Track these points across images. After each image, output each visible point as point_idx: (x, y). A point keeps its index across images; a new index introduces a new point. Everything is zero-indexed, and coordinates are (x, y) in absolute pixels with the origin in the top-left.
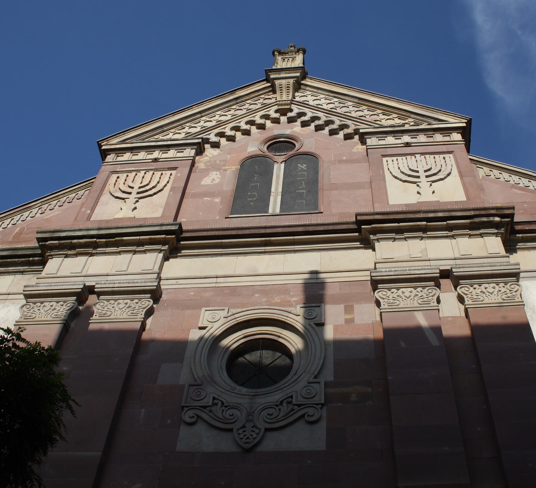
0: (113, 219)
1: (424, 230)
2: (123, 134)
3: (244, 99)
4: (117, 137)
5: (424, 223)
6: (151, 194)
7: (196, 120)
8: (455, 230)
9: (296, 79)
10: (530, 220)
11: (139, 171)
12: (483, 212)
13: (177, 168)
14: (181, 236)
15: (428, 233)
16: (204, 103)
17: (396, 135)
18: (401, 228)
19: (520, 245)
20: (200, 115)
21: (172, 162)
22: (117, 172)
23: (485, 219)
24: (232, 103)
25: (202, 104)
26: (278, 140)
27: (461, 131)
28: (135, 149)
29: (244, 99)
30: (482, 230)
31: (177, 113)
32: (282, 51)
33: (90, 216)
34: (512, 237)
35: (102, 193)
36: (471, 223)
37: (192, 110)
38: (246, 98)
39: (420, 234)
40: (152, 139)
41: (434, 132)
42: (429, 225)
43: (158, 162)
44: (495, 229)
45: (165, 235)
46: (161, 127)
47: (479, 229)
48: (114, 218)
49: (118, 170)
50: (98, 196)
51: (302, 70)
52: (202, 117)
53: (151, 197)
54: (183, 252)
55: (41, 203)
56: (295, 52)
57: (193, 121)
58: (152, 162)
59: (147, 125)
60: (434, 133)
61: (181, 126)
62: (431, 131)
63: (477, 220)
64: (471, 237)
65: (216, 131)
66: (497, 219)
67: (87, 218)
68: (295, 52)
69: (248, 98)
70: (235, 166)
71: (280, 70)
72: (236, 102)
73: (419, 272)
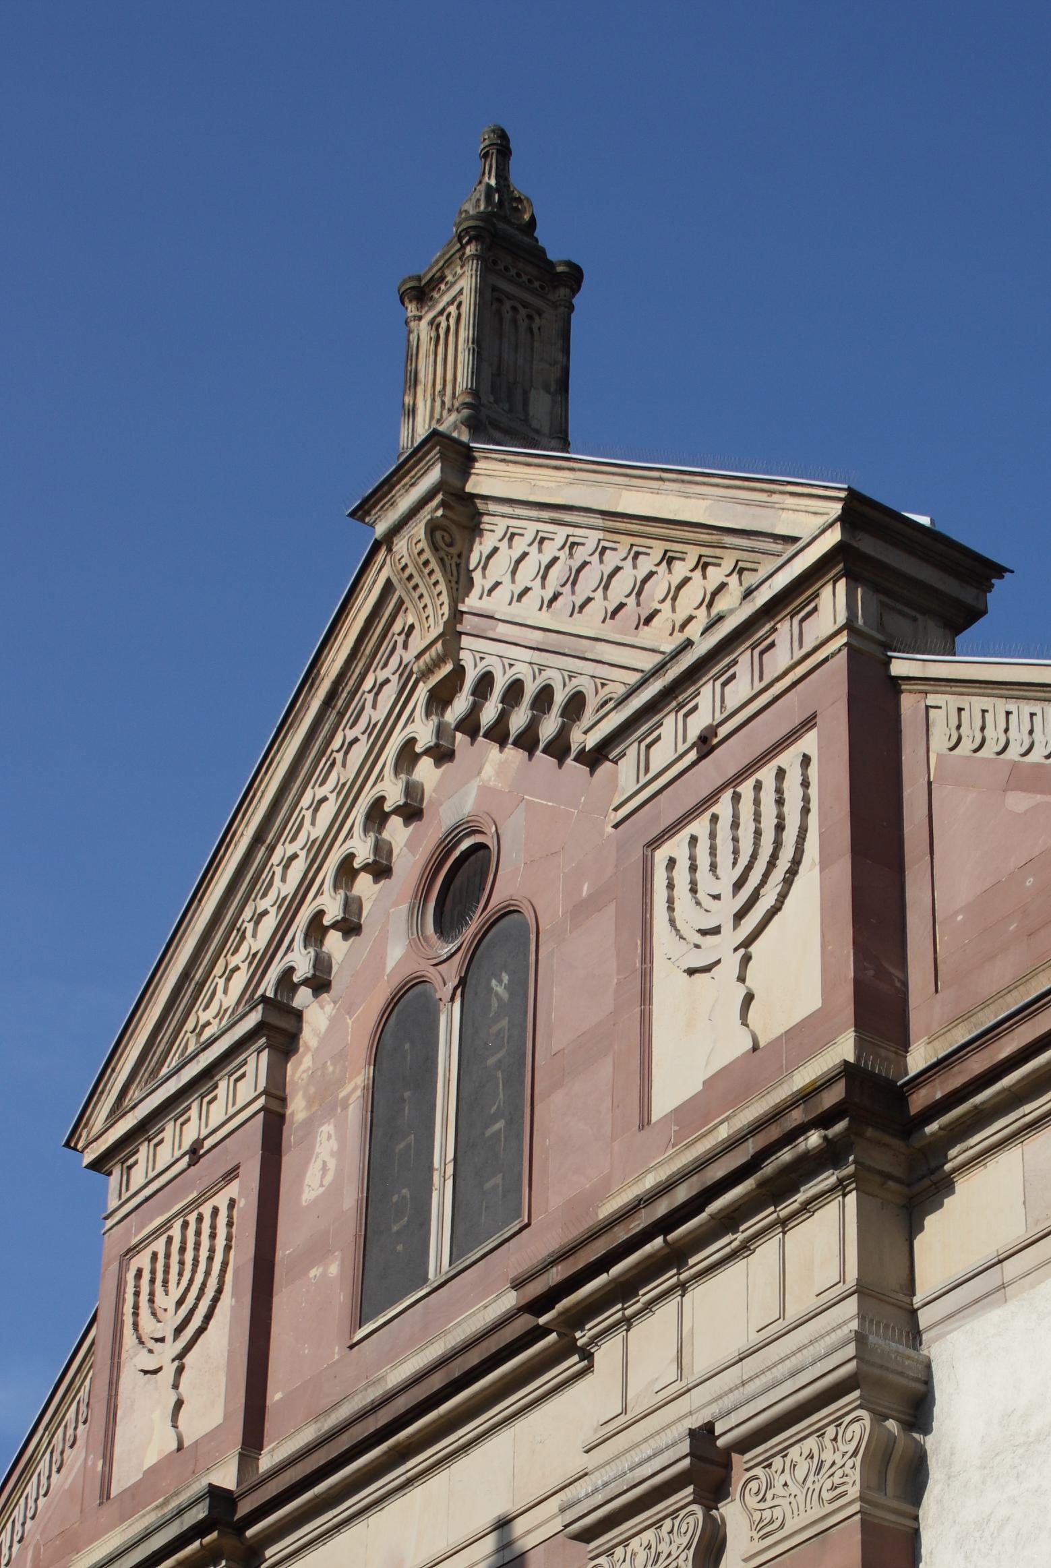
0: (141, 1476)
1: (676, 1257)
2: (109, 1070)
3: (351, 682)
4: (102, 1093)
5: (658, 1242)
6: (200, 1327)
7: (264, 876)
8: (743, 1224)
9: (440, 497)
10: (940, 1057)
11: (167, 1225)
12: (774, 1133)
13: (237, 1167)
14: (235, 1519)
15: (692, 1261)
16: (255, 786)
17: (680, 699)
18: (622, 1279)
19: (957, 1155)
20: (263, 849)
21: (228, 1140)
22: (135, 1248)
23: (786, 1155)
24: (327, 726)
25: (251, 794)
26: (457, 853)
27: (841, 565)
28: (148, 1123)
29: (351, 682)
30: (802, 1189)
31: (204, 886)
32: (425, 275)
33: (106, 1479)
34: (917, 1143)
35: (119, 1363)
36: (760, 1185)
37: (236, 845)
38: (357, 672)
39: (669, 1279)
40: (173, 1062)
41: (773, 618)
42: (676, 1241)
43: (202, 1160)
44: (831, 1171)
45: (199, 1540)
46: (185, 976)
47: (794, 1189)
48: (144, 1469)
49: (134, 1241)
50: (111, 1383)
51: (438, 448)
52: (271, 849)
53: (206, 1333)
54: (268, 1553)
55: (47, 1433)
56: (458, 255)
57: (258, 887)
58: (190, 1165)
59: (153, 993)
60: (772, 623)
61: (235, 932)
62: (762, 622)
63: (769, 1168)
64: (790, 1226)
65: (335, 861)
66: (814, 1139)
67: (101, 1497)
68: (458, 255)
69: (361, 665)
70: (359, 1073)
71: (386, 488)
72: (335, 712)
73: (647, 1470)
